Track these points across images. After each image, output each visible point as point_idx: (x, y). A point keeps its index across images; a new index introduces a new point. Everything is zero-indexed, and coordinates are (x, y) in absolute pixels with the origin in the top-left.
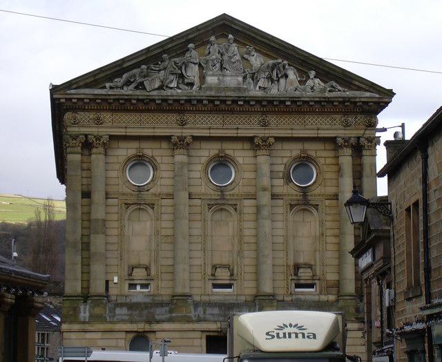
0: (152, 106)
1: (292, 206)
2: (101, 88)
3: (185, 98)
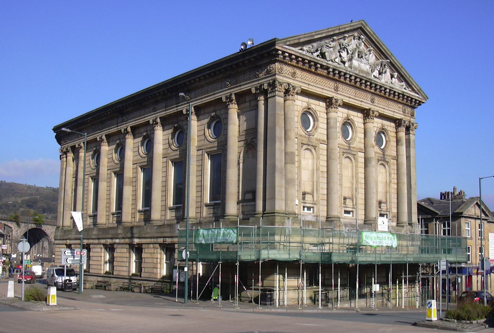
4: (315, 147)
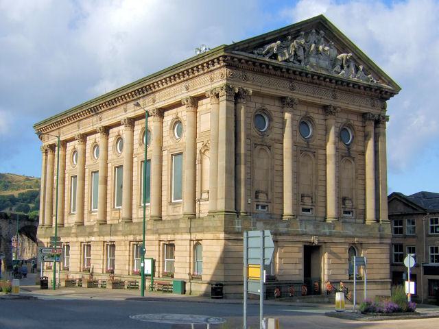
0: (278, 73)
1: (343, 157)
2: (250, 53)
3: (300, 70)
4: (269, 147)
